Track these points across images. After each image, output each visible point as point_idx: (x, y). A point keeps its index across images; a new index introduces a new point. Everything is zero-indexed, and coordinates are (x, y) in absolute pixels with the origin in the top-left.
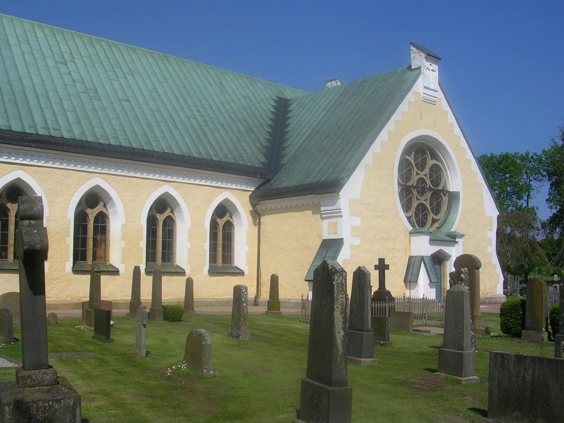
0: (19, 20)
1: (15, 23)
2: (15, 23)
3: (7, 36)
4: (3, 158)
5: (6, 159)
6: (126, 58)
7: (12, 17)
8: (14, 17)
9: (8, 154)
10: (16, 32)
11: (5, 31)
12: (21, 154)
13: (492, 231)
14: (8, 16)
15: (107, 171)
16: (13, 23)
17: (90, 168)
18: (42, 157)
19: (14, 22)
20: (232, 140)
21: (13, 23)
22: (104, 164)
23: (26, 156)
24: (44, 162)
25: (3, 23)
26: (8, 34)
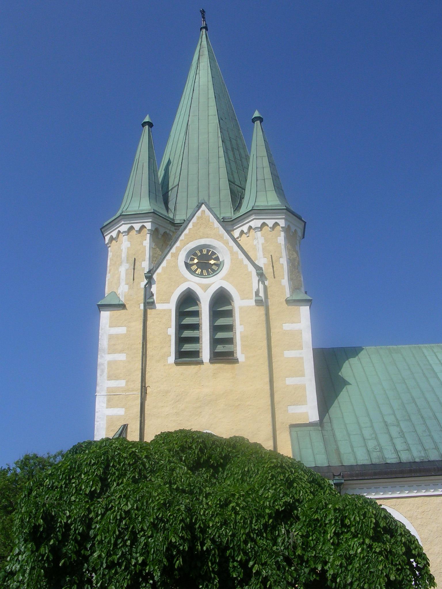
0: (438, 346)
1: (435, 350)
2: (435, 350)
3: (431, 365)
4: (439, 491)
5: (416, 493)
6: (166, 253)
7: (431, 345)
8: (433, 345)
9: (375, 489)
10: (438, 359)
11: (428, 361)
12: (431, 484)
13: (300, 322)
14: (426, 345)
15: (383, 495)
16: (433, 351)
17: (436, 491)
18: (396, 487)
19: (434, 349)
20: (214, 360)
21: (433, 351)
22: (387, 486)
23: (428, 486)
24: (408, 491)
25: (423, 353)
26: (431, 362)
